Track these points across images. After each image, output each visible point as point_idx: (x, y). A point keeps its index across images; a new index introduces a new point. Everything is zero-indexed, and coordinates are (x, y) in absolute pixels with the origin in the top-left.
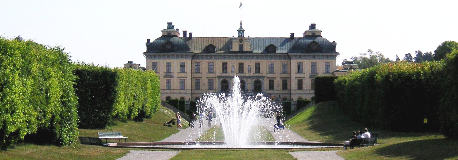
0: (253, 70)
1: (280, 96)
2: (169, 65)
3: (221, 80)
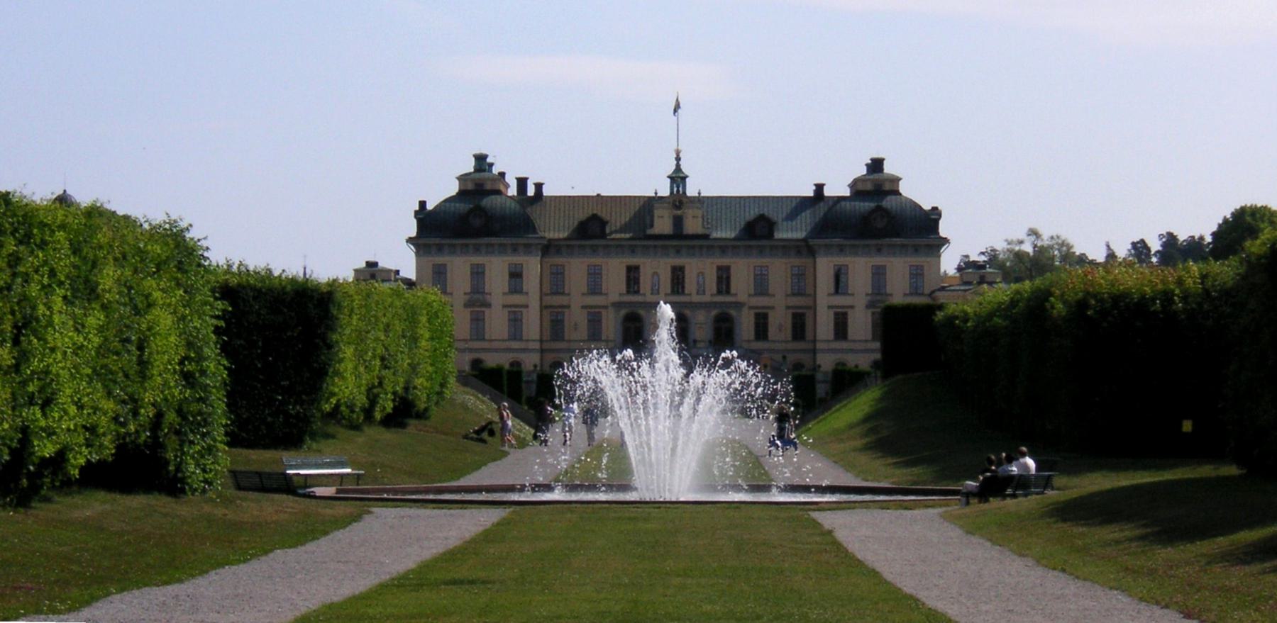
0: (711, 284)
1: (784, 357)
2: (478, 273)
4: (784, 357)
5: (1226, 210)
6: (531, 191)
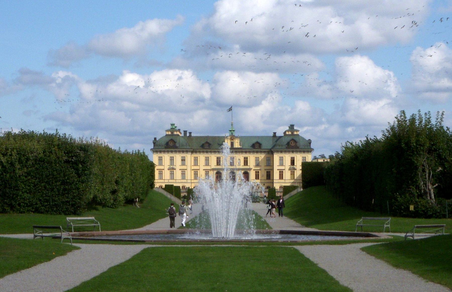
2: (172, 159)
6: (188, 135)
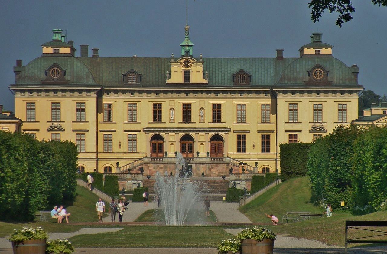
0: (179, 116)
1: (256, 163)
2: (56, 108)
3: (151, 135)
4: (256, 163)
5: (301, 47)
